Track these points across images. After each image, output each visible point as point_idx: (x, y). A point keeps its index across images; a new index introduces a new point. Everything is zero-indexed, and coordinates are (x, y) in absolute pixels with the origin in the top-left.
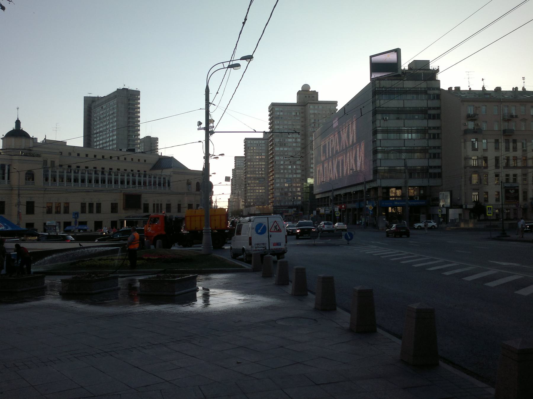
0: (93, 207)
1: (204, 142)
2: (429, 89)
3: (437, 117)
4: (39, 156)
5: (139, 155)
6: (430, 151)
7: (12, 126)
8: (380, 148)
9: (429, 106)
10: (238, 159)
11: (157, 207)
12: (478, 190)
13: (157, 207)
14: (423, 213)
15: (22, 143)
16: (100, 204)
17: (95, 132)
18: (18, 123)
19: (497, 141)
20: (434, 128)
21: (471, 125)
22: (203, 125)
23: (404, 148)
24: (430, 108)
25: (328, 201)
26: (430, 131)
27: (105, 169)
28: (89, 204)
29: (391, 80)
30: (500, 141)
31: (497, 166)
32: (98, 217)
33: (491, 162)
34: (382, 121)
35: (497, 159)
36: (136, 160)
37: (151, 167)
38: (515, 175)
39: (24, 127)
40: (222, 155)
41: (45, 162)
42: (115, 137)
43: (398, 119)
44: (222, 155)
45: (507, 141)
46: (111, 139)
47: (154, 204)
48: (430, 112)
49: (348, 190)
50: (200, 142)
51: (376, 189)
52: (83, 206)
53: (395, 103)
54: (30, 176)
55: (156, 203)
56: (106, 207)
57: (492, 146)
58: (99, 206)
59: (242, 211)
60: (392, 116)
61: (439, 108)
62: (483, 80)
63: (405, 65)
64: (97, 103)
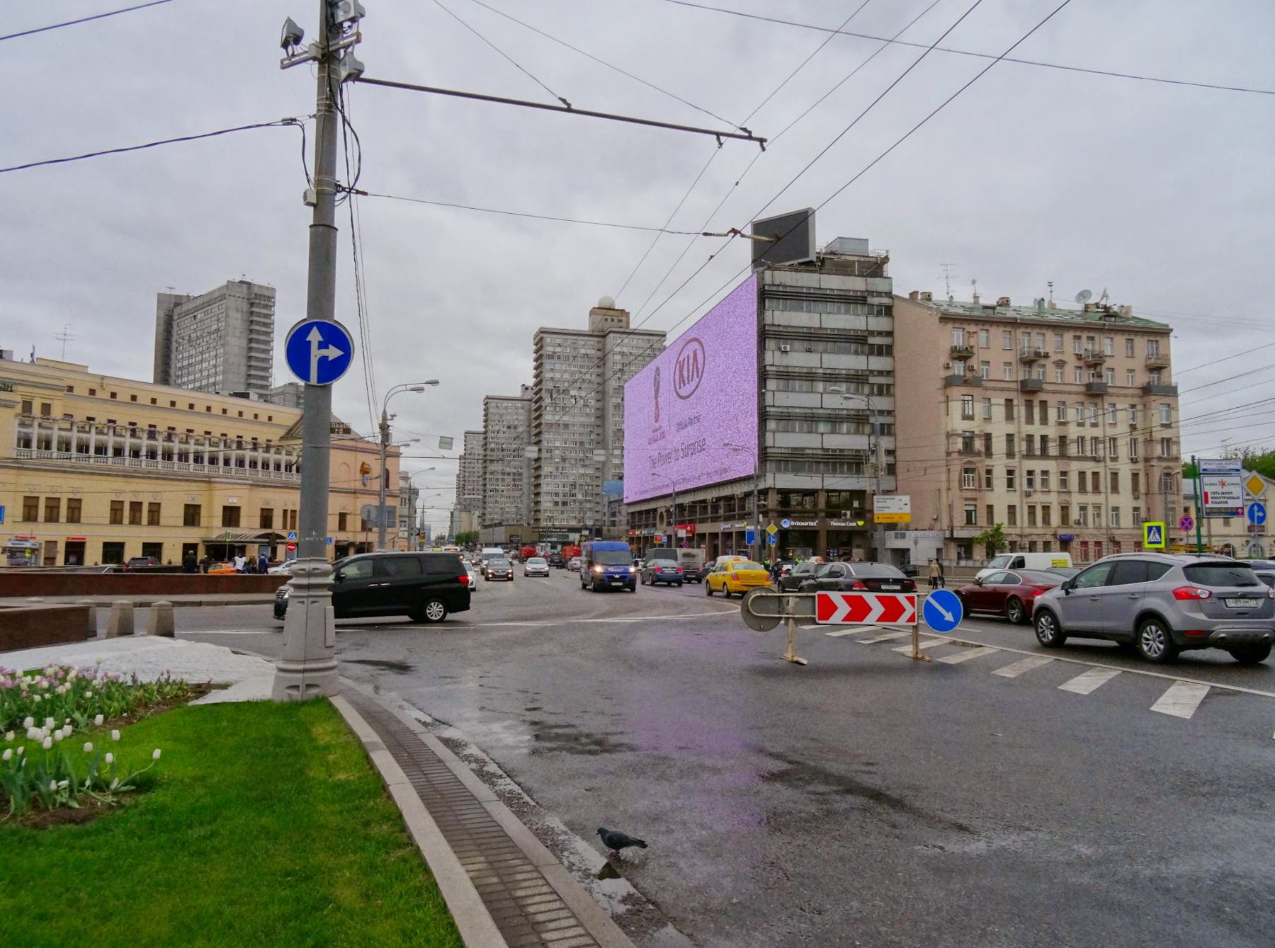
0: (140, 511)
1: (311, 127)
2: (871, 293)
3: (886, 351)
6: (872, 420)
8: (772, 409)
9: (870, 328)
12: (975, 499)
14: (859, 547)
16: (159, 504)
17: (179, 365)
19: (1009, 402)
20: (880, 373)
21: (958, 369)
22: (312, 34)
23: (821, 411)
24: (872, 333)
25: (655, 518)
26: (872, 380)
27: (177, 431)
28: (132, 503)
29: (796, 271)
30: (1015, 402)
31: (1010, 454)
32: (152, 535)
33: (999, 445)
34: (777, 354)
35: (1010, 438)
36: (248, 415)
37: (282, 432)
38: (1045, 473)
40: (435, 383)
41: (27, 406)
42: (219, 378)
43: (809, 351)
44: (435, 383)
45: (1029, 405)
46: (212, 380)
47: (285, 511)
48: (871, 340)
49: (700, 496)
50: (290, 122)
51: (764, 493)
52: (116, 508)
55: (290, 508)
56: (173, 512)
57: (999, 412)
58: (155, 509)
59: (476, 534)
60: (797, 344)
61: (890, 334)
62: (974, 282)
64: (185, 308)
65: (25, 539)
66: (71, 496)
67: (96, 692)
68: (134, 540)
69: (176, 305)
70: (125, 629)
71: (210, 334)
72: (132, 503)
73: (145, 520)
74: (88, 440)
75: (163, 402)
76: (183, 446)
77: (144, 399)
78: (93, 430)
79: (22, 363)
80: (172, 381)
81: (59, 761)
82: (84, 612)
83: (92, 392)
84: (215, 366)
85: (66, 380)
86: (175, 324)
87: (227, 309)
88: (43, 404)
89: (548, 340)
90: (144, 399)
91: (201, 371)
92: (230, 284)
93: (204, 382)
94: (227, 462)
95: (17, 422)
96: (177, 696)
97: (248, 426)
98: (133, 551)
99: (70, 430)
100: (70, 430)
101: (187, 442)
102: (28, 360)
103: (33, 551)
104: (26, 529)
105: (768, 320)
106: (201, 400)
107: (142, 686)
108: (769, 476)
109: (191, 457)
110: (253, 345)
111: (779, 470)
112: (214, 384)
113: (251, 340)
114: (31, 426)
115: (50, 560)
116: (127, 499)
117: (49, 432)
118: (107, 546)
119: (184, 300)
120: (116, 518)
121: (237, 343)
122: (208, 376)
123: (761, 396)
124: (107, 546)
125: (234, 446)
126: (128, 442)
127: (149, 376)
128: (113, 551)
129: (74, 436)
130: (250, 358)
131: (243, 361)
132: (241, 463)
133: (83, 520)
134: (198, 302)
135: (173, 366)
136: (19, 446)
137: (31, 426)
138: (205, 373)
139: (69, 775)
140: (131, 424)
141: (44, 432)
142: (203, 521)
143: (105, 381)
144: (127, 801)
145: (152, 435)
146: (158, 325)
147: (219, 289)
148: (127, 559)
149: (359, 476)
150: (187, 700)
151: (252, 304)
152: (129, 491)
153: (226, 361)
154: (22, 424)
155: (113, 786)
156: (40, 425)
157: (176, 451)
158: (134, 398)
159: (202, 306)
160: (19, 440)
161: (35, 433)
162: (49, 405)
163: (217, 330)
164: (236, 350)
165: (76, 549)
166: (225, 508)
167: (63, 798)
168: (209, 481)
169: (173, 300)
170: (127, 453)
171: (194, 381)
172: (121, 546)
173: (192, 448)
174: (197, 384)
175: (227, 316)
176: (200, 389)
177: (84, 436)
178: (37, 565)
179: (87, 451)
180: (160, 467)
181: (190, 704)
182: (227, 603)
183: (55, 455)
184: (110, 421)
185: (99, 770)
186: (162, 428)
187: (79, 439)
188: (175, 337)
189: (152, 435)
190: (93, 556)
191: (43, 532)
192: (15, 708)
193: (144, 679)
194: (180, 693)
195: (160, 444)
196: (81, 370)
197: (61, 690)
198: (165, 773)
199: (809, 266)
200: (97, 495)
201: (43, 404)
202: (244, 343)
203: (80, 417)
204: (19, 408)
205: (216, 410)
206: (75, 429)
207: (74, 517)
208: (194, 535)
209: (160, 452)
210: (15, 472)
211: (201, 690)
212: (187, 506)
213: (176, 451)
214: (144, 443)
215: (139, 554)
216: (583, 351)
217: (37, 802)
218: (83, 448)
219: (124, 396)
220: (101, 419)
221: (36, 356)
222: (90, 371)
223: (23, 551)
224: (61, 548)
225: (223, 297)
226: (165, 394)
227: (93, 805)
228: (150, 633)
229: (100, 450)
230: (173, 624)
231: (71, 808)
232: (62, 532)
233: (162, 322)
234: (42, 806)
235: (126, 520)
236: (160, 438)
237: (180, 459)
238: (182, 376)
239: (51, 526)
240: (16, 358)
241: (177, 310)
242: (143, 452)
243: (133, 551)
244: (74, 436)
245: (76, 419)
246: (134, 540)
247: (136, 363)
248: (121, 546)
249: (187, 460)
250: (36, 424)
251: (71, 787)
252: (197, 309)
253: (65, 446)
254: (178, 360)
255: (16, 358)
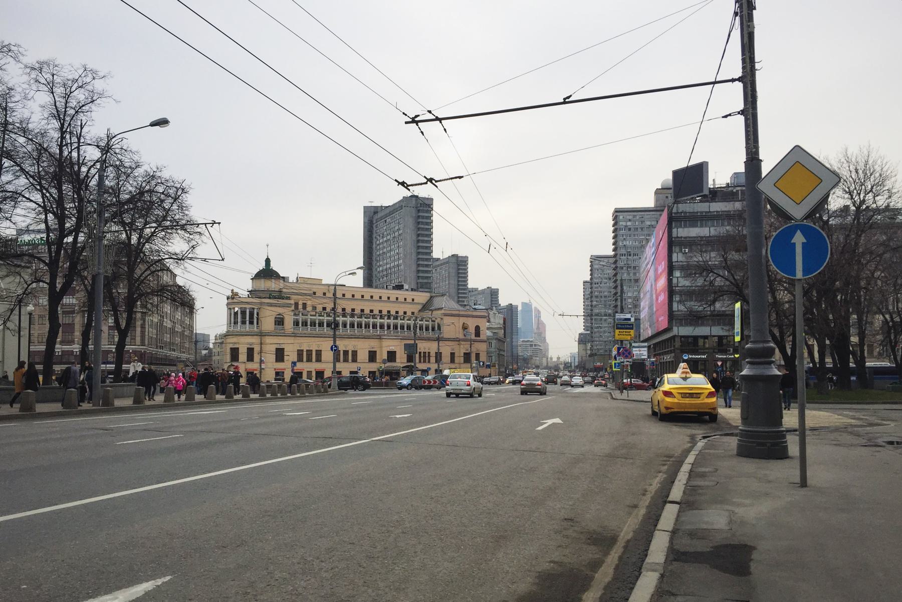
5: (406, 293)
7: (262, 265)
10: (406, 225)
11: (424, 356)
13: (424, 356)
15: (272, 285)
18: (268, 261)
32: (319, 366)
34: (680, 255)
36: (401, 299)
37: (420, 307)
39: (274, 266)
41: (296, 304)
42: (401, 261)
52: (300, 353)
53: (694, 232)
56: (363, 356)
58: (355, 353)
64: (380, 215)
83: (324, 294)
89: (621, 217)
94: (389, 327)
105: (674, 235)
108: (675, 329)
110: (420, 238)
111: (681, 325)
113: (418, 235)
119: (379, 209)
121: (409, 236)
123: (670, 281)
130: (418, 247)
131: (414, 250)
132: (396, 327)
134: (387, 211)
149: (461, 330)
151: (419, 211)
154: (295, 315)
161: (300, 318)
168: (380, 338)
188: (374, 236)
199: (705, 199)
202: (414, 237)
204: (293, 308)
208: (374, 367)
216: (648, 223)
224: (314, 374)
237: (320, 325)
241: (376, 217)
252: (386, 216)
253: (313, 324)
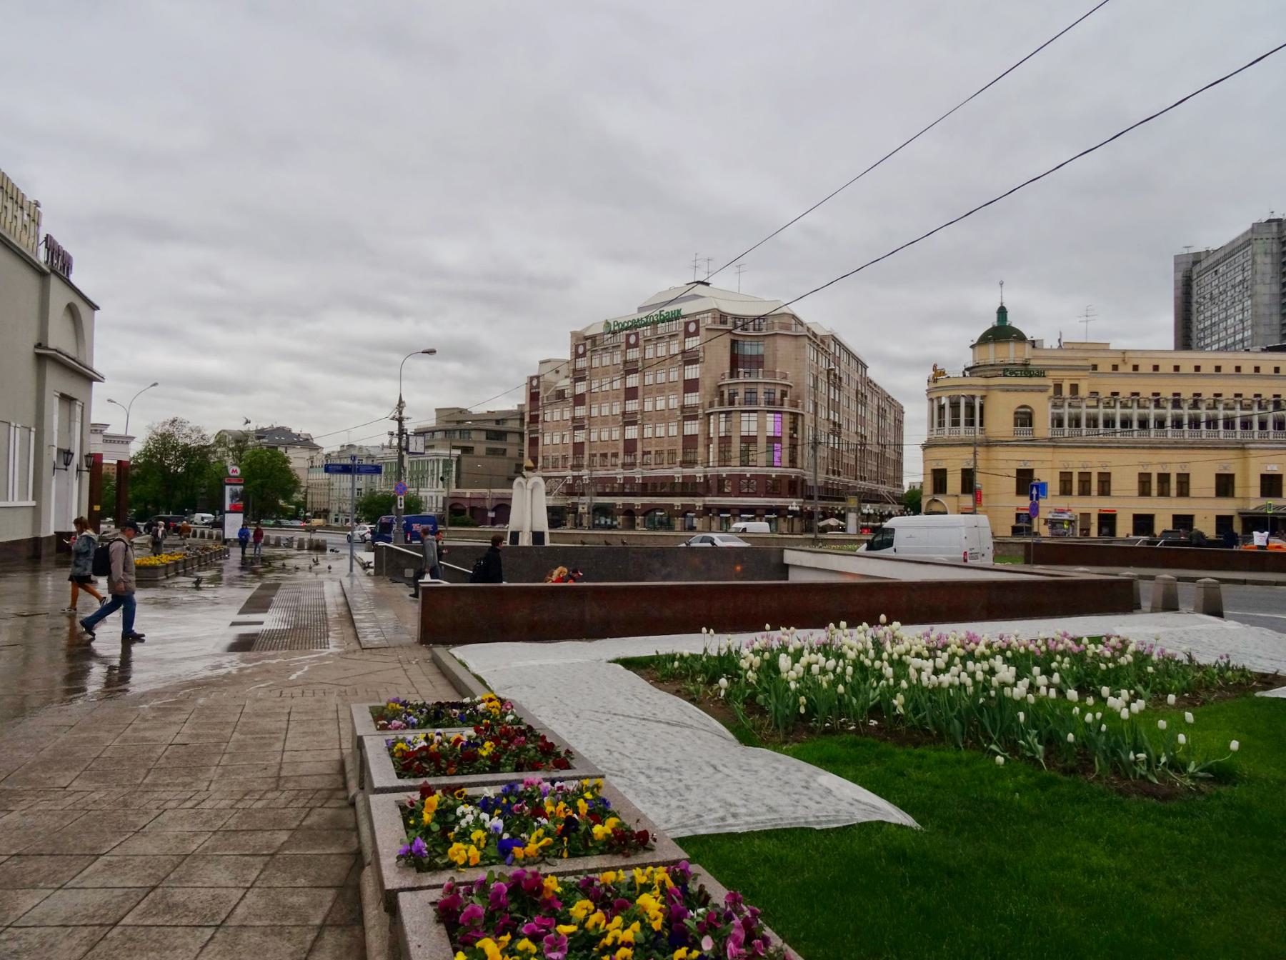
4: (1041, 373)
7: (991, 321)
15: (1010, 353)
16: (1188, 475)
18: (1002, 312)
27: (1204, 397)
28: (1160, 475)
39: (1013, 321)
41: (1058, 388)
42: (1248, 333)
46: (1239, 337)
52: (1144, 480)
54: (1024, 418)
56: (1203, 482)
58: (1184, 480)
63: (1267, 533)
64: (1204, 264)
65: (1062, 512)
66: (1102, 470)
67: (1155, 666)
68: (1164, 512)
69: (1195, 263)
70: (1169, 604)
71: (1234, 287)
72: (1160, 475)
73: (1174, 492)
74: (1114, 415)
75: (1187, 368)
76: (1211, 412)
77: (1166, 368)
78: (1118, 405)
79: (1051, 349)
80: (1194, 346)
81: (1135, 732)
82: (1129, 584)
83: (1115, 367)
84: (1242, 321)
85: (1090, 358)
86: (1194, 283)
87: (1254, 255)
88: (1072, 385)
90: (1166, 368)
91: (1226, 329)
92: (1256, 228)
93: (1230, 341)
94: (1263, 425)
95: (1050, 404)
96: (1240, 683)
97: (1267, 383)
98: (1163, 523)
99: (1097, 407)
100: (1097, 407)
101: (1215, 408)
102: (1056, 345)
103: (1071, 522)
104: (1063, 502)
106: (1228, 361)
107: (1200, 667)
109: (1221, 423)
112: (1242, 341)
114: (1062, 406)
115: (1085, 531)
116: (1154, 471)
117: (1146, 411)
118: (1137, 518)
120: (1144, 490)
122: (1235, 333)
124: (1137, 518)
125: (1271, 407)
126: (1152, 412)
127: (1170, 344)
128: (1143, 523)
129: (1101, 412)
133: (1113, 493)
134: (1218, 256)
135: (1194, 329)
136: (1016, 425)
137: (1062, 406)
138: (1231, 331)
139: (1147, 750)
140: (1154, 394)
141: (1073, 411)
142: (1238, 492)
143: (1127, 355)
144: (1203, 787)
145: (1177, 403)
146: (1176, 289)
147: (1242, 236)
148: (1158, 530)
150: (1255, 689)
152: (1156, 463)
153: (1255, 315)
154: (1055, 406)
155: (1191, 769)
156: (1070, 405)
157: (1203, 418)
158: (1156, 368)
159: (1225, 258)
160: (1016, 419)
161: (1066, 412)
162: (1076, 386)
163: (1244, 280)
164: (1266, 299)
165: (1108, 521)
166: (1263, 476)
167: (1142, 770)
168: (1242, 448)
169: (1191, 260)
170: (1152, 425)
171: (1219, 341)
172: (1150, 518)
173: (1221, 413)
174: (1223, 344)
175: (1254, 262)
176: (1226, 348)
177: (1109, 411)
178: (1074, 537)
179: (1113, 426)
180: (1186, 436)
181: (1258, 694)
182: (1277, 584)
183: (1084, 433)
184: (1134, 394)
185: (1173, 750)
186: (1187, 395)
187: (1106, 415)
188: (1195, 298)
189: (1177, 403)
190: (1124, 528)
191: (1077, 505)
192: (1082, 672)
193: (1202, 660)
194: (1244, 680)
195: (1203, 413)
196: (1104, 348)
197: (1123, 661)
198: (1246, 768)
200: (1125, 468)
201: (1072, 385)
203: (1105, 393)
205: (1247, 369)
206: (1101, 405)
207: (1105, 490)
208: (1228, 507)
209: (1186, 421)
210: (1051, 450)
211: (1270, 680)
212: (1219, 476)
213: (1203, 418)
214: (1169, 412)
215: (1169, 526)
217: (1120, 769)
218: (1109, 423)
219: (1146, 368)
220: (1125, 393)
221: (1063, 340)
222: (1111, 347)
223: (1062, 522)
225: (1248, 243)
226: (1187, 359)
227: (1172, 784)
228: (1196, 610)
229: (1126, 423)
230: (1220, 603)
231: (1150, 782)
232: (1094, 505)
233: (1180, 284)
234: (1123, 774)
235: (1154, 491)
236: (1186, 406)
237: (1208, 427)
238: (1205, 338)
239: (1085, 499)
240: (1046, 346)
241: (1197, 269)
242: (1169, 423)
243: (1163, 523)
244: (1101, 412)
245: (1102, 395)
246: (1164, 512)
247: (1154, 330)
248: (1150, 518)
249: (1216, 426)
250: (1066, 404)
251: (1148, 761)
252: (1218, 263)
254: (1201, 321)
255: (1046, 346)
